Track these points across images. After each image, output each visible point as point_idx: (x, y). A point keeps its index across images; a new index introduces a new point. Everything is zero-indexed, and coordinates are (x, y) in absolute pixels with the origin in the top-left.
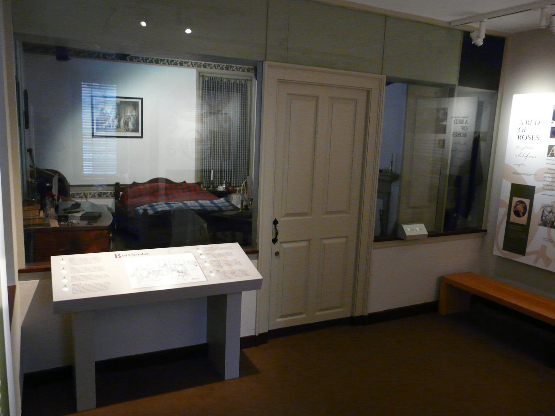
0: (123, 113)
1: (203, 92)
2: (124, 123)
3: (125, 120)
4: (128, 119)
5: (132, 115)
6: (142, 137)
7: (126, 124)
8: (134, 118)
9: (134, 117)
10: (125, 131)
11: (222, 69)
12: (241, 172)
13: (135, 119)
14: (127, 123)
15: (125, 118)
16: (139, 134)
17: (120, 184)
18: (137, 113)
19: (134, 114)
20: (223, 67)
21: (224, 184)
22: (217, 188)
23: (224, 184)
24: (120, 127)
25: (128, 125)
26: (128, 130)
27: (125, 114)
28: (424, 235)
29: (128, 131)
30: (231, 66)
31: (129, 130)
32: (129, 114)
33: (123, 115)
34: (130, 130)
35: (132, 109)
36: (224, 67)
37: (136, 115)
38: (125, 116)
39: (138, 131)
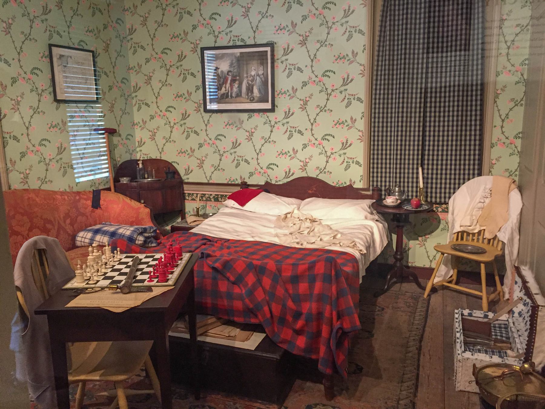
0: (245, 73)
1: (482, 79)
2: (247, 89)
3: (248, 83)
4: (252, 81)
5: (258, 75)
6: (272, 110)
7: (250, 89)
8: (261, 79)
9: (261, 76)
10: (249, 101)
11: (208, 201)
12: (390, 87)
13: (262, 81)
14: (251, 88)
15: (248, 80)
16: (268, 106)
17: (248, 183)
18: (265, 69)
19: (261, 72)
20: (209, 197)
21: (397, 194)
22: (384, 201)
23: (397, 194)
24: (241, 95)
25: (252, 92)
26: (252, 99)
27: (247, 74)
28: (525, 113)
29: (252, 101)
30: (188, 194)
31: (254, 99)
32: (253, 73)
33: (245, 75)
34: (256, 99)
35: (258, 66)
36: (211, 197)
37: (263, 74)
38: (247, 77)
39: (267, 101)
